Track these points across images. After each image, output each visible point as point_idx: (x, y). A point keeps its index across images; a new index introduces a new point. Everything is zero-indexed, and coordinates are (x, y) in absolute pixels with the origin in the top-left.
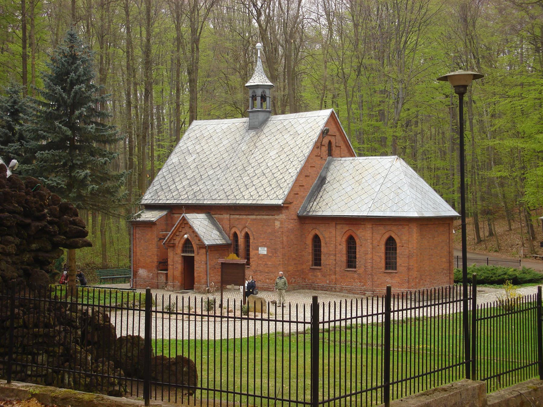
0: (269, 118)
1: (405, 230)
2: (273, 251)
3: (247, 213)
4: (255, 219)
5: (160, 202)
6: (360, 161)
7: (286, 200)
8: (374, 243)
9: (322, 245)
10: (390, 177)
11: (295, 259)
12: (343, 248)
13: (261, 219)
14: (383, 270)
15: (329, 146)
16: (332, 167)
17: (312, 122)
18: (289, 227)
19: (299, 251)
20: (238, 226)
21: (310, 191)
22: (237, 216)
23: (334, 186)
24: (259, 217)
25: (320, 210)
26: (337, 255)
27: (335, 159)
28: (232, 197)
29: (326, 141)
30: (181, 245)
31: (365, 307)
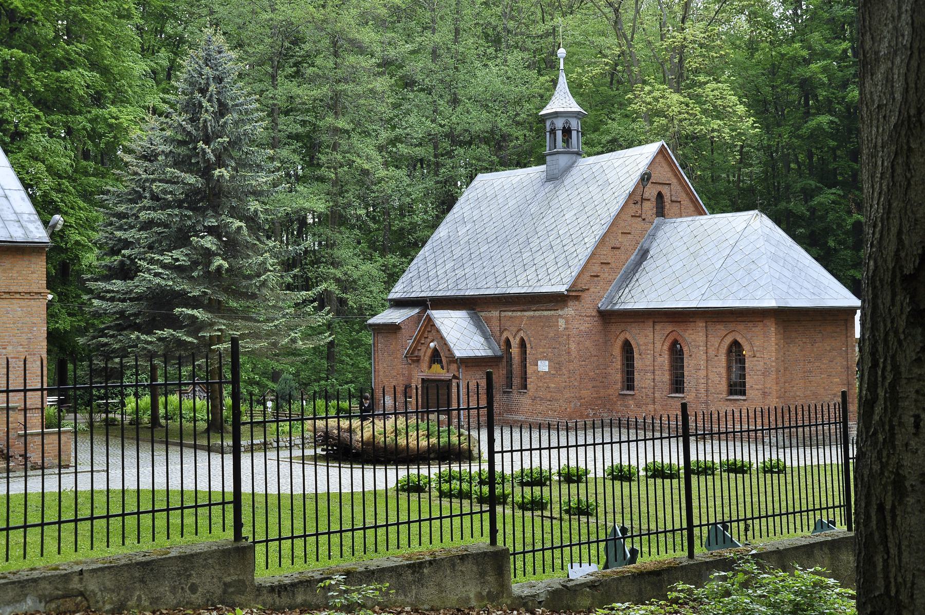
0: (575, 162)
1: (758, 329)
2: (556, 366)
3: (522, 307)
4: (533, 317)
5: (413, 295)
6: (702, 222)
7: (574, 284)
8: (710, 351)
9: (641, 354)
10: (741, 245)
11: (594, 379)
12: (664, 360)
13: (540, 317)
14: (724, 395)
15: (651, 202)
16: (660, 233)
17: (631, 164)
18: (582, 328)
19: (602, 367)
20: (511, 328)
21: (622, 272)
22: (510, 313)
23: (658, 263)
24: (537, 313)
25: (632, 300)
26: (657, 373)
27: (667, 220)
28: (502, 284)
29: (651, 192)
30: (427, 358)
31: (724, 451)
